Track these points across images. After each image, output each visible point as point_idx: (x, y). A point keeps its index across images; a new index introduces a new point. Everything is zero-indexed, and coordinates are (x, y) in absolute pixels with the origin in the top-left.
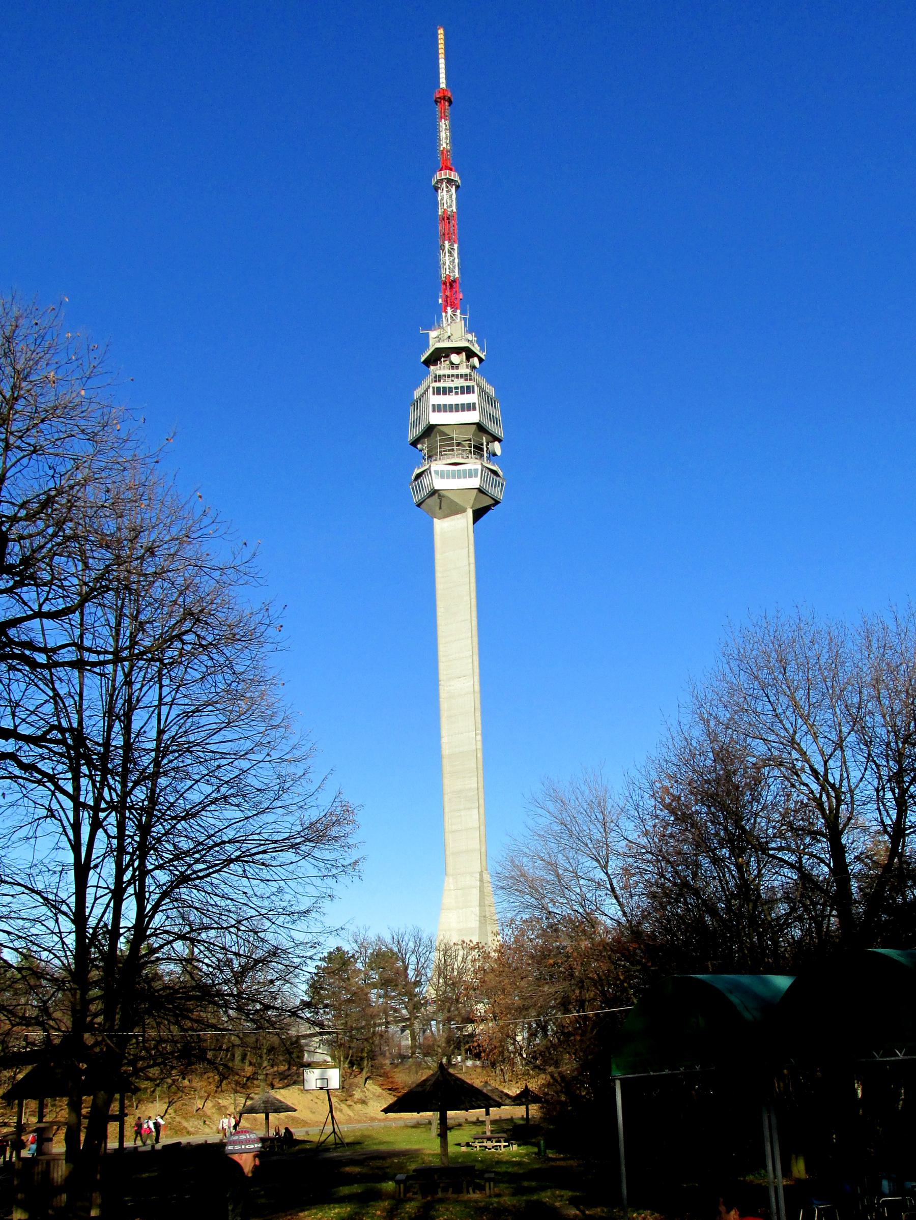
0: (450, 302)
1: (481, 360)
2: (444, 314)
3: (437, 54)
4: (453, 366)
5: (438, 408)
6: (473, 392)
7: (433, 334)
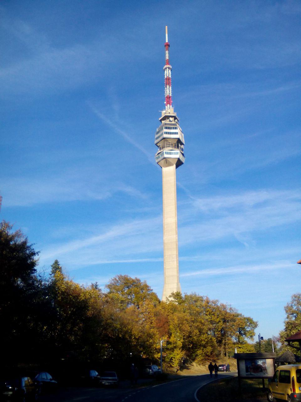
0: (168, 103)
1: (178, 121)
2: (166, 88)
3: (165, 32)
4: (170, 121)
5: (166, 133)
6: (177, 129)
7: (164, 112)
